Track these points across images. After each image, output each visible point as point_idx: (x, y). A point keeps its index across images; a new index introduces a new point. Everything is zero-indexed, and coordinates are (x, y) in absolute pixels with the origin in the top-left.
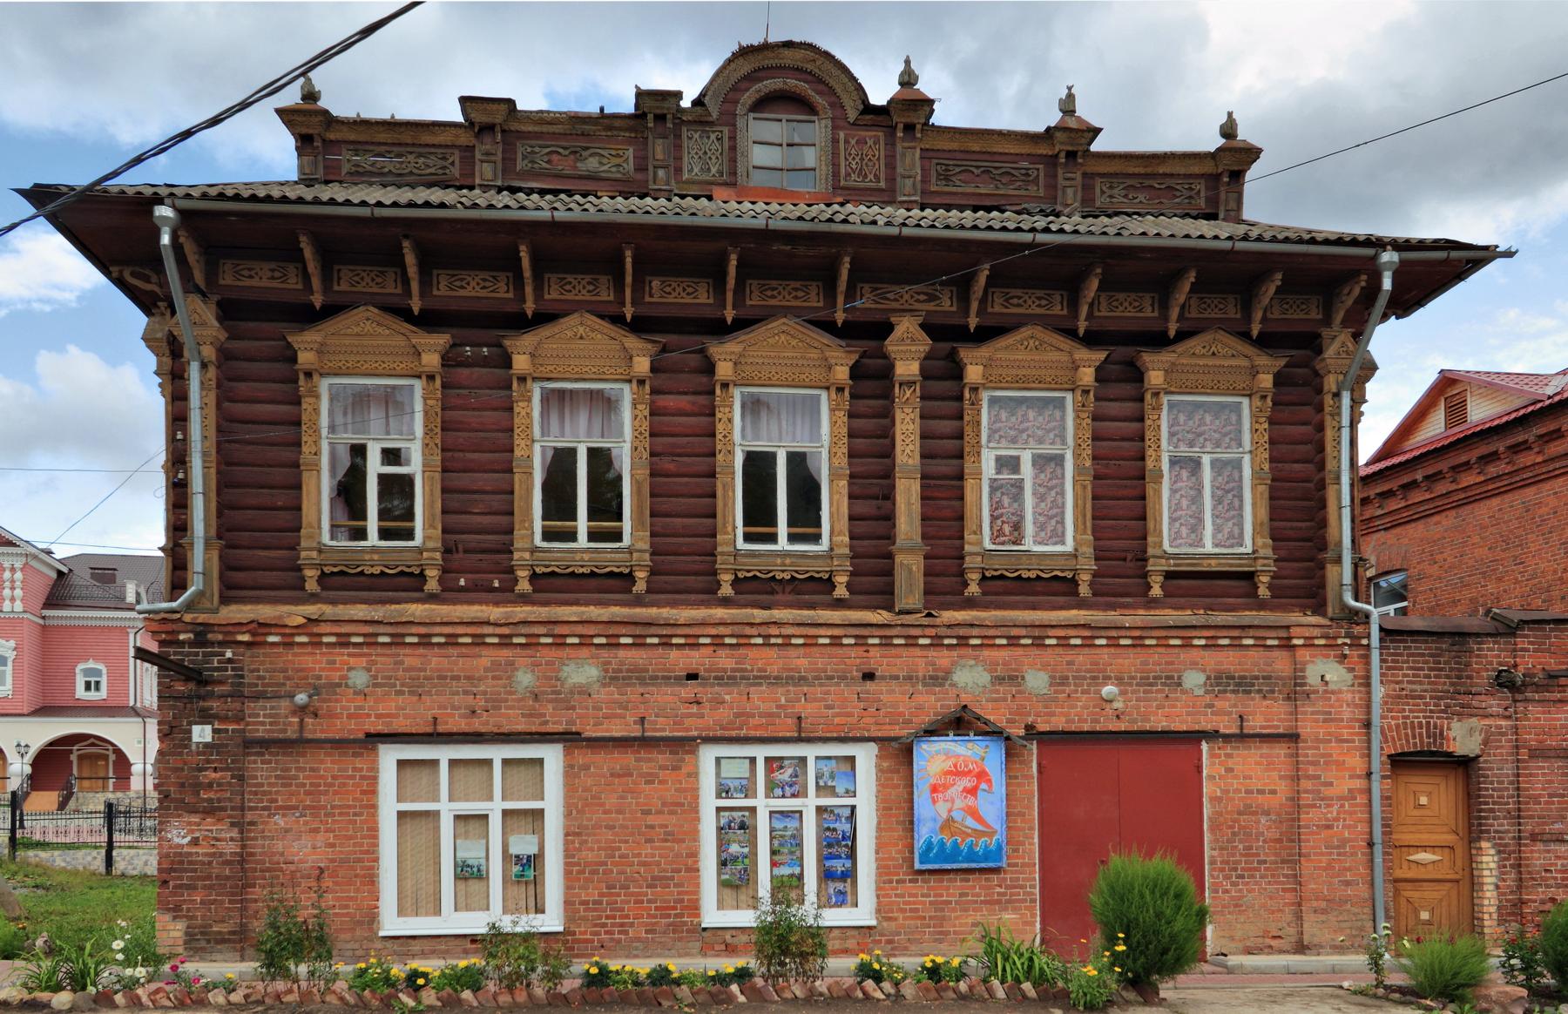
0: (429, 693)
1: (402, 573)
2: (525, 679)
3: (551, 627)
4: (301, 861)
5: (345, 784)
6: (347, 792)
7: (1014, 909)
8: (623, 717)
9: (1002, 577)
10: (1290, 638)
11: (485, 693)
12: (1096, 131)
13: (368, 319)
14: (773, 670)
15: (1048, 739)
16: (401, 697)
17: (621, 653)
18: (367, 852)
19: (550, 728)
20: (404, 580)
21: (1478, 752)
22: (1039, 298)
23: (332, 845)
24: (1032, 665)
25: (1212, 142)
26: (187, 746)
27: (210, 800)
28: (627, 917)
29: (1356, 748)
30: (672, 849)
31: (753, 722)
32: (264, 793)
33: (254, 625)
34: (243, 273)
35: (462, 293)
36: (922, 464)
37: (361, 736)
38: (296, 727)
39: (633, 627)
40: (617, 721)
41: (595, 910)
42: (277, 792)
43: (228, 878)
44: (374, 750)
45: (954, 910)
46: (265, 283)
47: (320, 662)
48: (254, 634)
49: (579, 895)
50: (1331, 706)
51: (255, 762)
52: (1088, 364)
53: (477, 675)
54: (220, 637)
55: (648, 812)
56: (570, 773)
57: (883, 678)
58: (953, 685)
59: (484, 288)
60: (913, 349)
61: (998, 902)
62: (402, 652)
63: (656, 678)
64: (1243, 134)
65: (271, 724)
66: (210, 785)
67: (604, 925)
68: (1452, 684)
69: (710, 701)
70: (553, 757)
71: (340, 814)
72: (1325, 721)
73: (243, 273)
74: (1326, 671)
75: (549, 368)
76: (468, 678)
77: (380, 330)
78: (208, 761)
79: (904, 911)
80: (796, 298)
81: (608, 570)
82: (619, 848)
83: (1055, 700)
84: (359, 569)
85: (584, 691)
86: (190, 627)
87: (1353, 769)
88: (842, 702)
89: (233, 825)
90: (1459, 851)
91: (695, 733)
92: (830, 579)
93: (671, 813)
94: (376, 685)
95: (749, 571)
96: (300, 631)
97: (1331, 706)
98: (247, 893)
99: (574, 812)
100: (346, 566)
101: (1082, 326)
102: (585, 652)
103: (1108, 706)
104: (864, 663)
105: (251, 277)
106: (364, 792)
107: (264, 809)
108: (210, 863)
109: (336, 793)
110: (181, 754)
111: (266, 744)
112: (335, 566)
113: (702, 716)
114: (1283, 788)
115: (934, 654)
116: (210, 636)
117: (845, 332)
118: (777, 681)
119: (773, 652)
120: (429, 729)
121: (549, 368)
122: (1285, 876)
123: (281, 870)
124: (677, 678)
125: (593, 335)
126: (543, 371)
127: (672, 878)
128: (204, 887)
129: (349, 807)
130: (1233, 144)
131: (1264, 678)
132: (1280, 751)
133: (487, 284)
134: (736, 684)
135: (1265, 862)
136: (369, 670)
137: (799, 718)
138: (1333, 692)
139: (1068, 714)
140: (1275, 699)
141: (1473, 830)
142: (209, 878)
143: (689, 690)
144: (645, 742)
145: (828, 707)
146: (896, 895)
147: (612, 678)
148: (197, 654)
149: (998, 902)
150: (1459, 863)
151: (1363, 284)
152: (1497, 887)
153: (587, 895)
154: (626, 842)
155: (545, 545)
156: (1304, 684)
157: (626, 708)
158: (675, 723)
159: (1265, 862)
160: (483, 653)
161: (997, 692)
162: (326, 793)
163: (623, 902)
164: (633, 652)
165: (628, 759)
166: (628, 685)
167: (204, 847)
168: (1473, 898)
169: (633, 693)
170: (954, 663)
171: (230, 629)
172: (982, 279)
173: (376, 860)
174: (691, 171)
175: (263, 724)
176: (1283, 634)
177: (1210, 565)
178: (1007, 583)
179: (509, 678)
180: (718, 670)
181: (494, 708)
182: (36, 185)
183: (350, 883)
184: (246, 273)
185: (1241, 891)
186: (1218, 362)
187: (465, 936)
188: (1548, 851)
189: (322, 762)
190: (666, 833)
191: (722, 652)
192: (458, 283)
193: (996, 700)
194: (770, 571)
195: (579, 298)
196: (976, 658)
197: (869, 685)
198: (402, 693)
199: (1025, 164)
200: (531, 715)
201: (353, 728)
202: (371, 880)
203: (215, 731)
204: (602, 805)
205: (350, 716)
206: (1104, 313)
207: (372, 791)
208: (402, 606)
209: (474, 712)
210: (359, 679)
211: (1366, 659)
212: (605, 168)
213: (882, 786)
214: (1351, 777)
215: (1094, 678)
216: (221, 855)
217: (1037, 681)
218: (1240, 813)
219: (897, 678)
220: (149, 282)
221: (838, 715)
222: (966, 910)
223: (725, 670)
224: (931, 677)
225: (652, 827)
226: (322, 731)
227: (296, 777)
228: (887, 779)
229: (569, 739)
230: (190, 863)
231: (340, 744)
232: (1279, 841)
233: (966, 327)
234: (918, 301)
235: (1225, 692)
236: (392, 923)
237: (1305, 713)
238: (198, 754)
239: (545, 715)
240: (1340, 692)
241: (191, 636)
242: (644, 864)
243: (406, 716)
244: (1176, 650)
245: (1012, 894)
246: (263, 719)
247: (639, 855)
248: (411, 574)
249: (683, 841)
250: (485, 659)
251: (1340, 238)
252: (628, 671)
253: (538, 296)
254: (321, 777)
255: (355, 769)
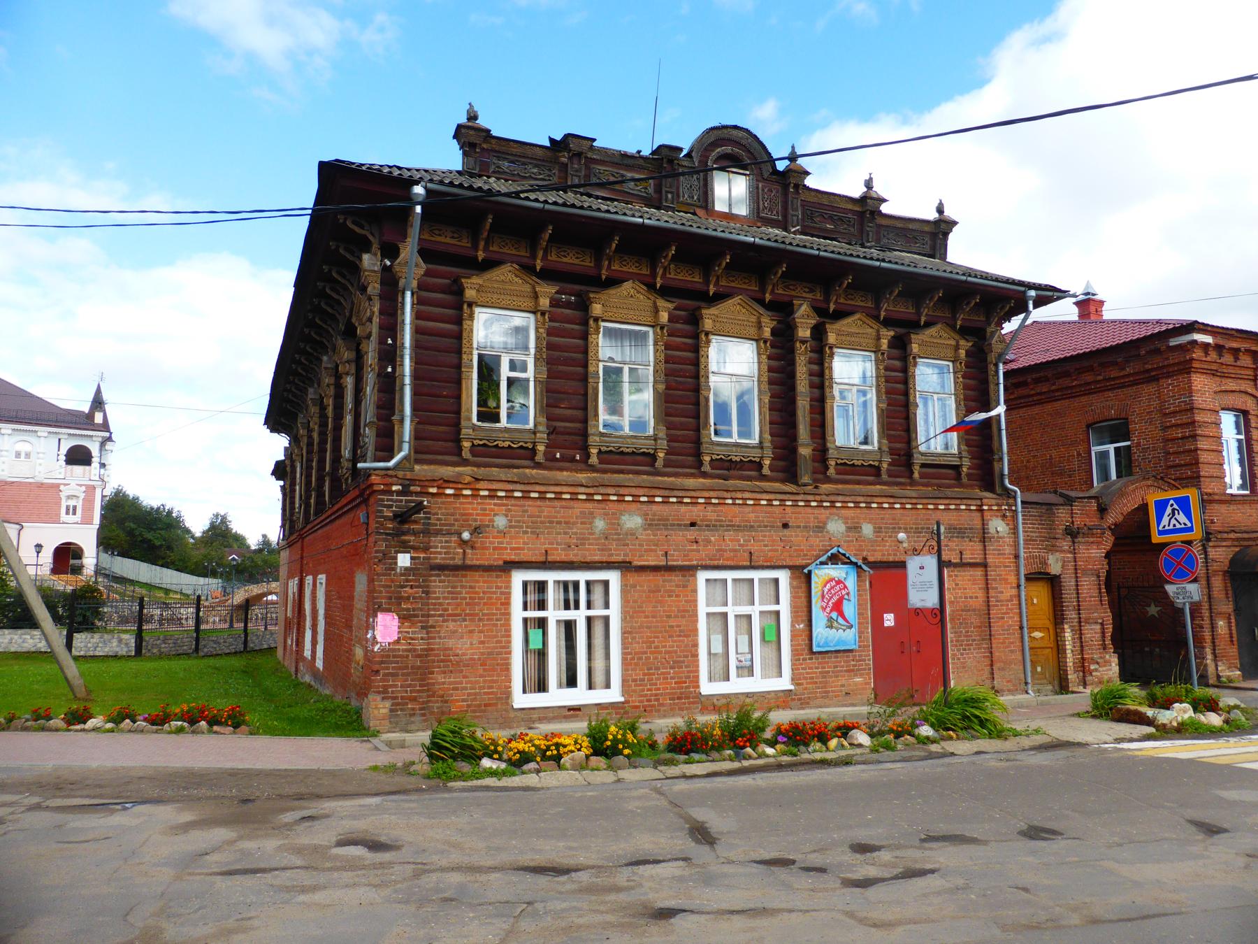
0: (543, 533)
1: (521, 447)
2: (600, 524)
3: (617, 489)
4: (464, 654)
5: (491, 598)
6: (493, 604)
7: (861, 675)
8: (656, 551)
9: (845, 464)
10: (982, 505)
11: (576, 533)
12: (884, 200)
13: (510, 272)
14: (737, 521)
15: (874, 565)
16: (526, 536)
17: (654, 507)
18: (504, 647)
19: (614, 558)
20: (522, 451)
21: (1060, 572)
22: (862, 296)
23: (482, 642)
24: (865, 519)
25: (932, 215)
26: (394, 569)
27: (408, 610)
28: (659, 689)
29: (1011, 571)
30: (683, 641)
31: (727, 555)
32: (440, 604)
33: (441, 481)
34: (435, 231)
35: (565, 260)
36: (810, 392)
37: (501, 563)
38: (461, 556)
39: (663, 491)
40: (652, 554)
41: (641, 685)
42: (448, 604)
43: (419, 668)
44: (694, 576)
45: (831, 677)
46: (448, 240)
47: (476, 509)
48: (439, 487)
49: (631, 675)
50: (1000, 546)
51: (435, 581)
52: (887, 334)
53: (572, 520)
54: (418, 489)
55: (669, 617)
56: (624, 591)
57: (793, 527)
58: (827, 532)
59: (577, 258)
60: (809, 321)
61: (853, 671)
62: (527, 503)
63: (674, 525)
64: (947, 213)
65: (445, 553)
66: (408, 598)
67: (646, 695)
68: (1048, 533)
69: (703, 540)
70: (613, 577)
71: (488, 620)
72: (999, 554)
73: (435, 231)
74: (998, 526)
75: (610, 314)
76: (566, 523)
77: (517, 279)
78: (407, 581)
79: (806, 678)
80: (745, 283)
81: (642, 450)
82: (654, 642)
83: (876, 541)
84: (495, 443)
85: (632, 533)
86: (400, 481)
87: (1011, 583)
88: (762, 544)
89: (422, 627)
90: (1051, 631)
91: (695, 563)
92: (760, 462)
93: (683, 617)
94: (511, 527)
95: (718, 455)
96: (468, 487)
97: (1000, 546)
98: (429, 679)
99: (628, 617)
100: (488, 440)
101: (768, 297)
102: (634, 506)
103: (900, 545)
104: (783, 517)
105: (440, 235)
106: (502, 604)
107: (440, 616)
108: (407, 656)
109: (485, 604)
110: (390, 575)
111: (442, 568)
112: (481, 440)
113: (698, 551)
114: (981, 595)
115: (818, 512)
116: (412, 488)
117: (772, 307)
118: (738, 528)
119: (736, 509)
120: (542, 559)
121: (610, 314)
122: (984, 648)
123: (451, 661)
124: (685, 525)
125: (638, 295)
126: (607, 316)
127: (684, 662)
128: (403, 675)
129: (494, 614)
130: (942, 217)
131: (970, 529)
132: (979, 573)
133: (579, 256)
134: (717, 530)
135: (975, 640)
136: (506, 516)
137: (750, 553)
138: (1001, 538)
139: (882, 551)
140: (975, 542)
141: (1058, 618)
142: (407, 668)
143: (692, 534)
144: (669, 569)
145: (765, 546)
146: (803, 669)
147: (649, 525)
148: (401, 501)
149: (853, 671)
150: (1052, 638)
151: (550, 232)
152: (1072, 651)
153: (636, 675)
154: (658, 637)
155: (479, 424)
156: (988, 533)
157: (657, 545)
158: (684, 556)
159: (975, 640)
160: (576, 506)
161: (848, 536)
162: (479, 604)
163: (656, 679)
164: (661, 507)
165: (658, 578)
166: (658, 530)
167: (404, 645)
168: (1059, 658)
169: (661, 535)
170: (828, 518)
171: (427, 483)
172: (546, 236)
173: (510, 653)
174: (684, 197)
175: (440, 553)
176: (979, 503)
177: (940, 460)
178: (848, 468)
179: (591, 523)
180: (707, 520)
181: (582, 544)
182: (337, 160)
183: (494, 670)
184: (437, 232)
185: (964, 658)
186: (942, 342)
187: (565, 707)
188: (1091, 629)
189: (478, 582)
190: (680, 631)
191: (710, 508)
192: (562, 253)
193: (848, 541)
194: (729, 456)
195: (631, 270)
196: (838, 515)
197: (786, 532)
198: (526, 532)
199: (850, 216)
200: (602, 550)
201: (495, 558)
202: (506, 668)
203: (412, 558)
204: (644, 612)
205: (495, 549)
206: (672, 276)
207: (507, 603)
208: (432, 467)
209: (569, 546)
210: (501, 522)
211: (1015, 518)
212: (639, 188)
213: (794, 597)
214: (1011, 588)
215: (894, 528)
216: (415, 650)
217: (868, 530)
218: (962, 610)
219: (799, 527)
220: (363, 229)
221: (771, 550)
222: (837, 677)
223: (711, 521)
224: (817, 527)
225: (672, 627)
226: (477, 560)
227: (461, 593)
228: (795, 593)
229: (624, 567)
230: (394, 656)
231: (488, 569)
232: (980, 627)
233: (476, 257)
234: (805, 292)
235: (952, 537)
236: (521, 700)
237: (989, 550)
238: (402, 575)
239: (611, 550)
240: (1004, 537)
241: (400, 487)
242: (669, 652)
243: (529, 549)
244: (930, 512)
245: (859, 665)
246: (442, 549)
247: (665, 646)
248: (527, 448)
249: (689, 636)
250: (578, 508)
251: (1008, 280)
252: (659, 520)
253: (544, 258)
254: (476, 593)
255: (497, 587)
